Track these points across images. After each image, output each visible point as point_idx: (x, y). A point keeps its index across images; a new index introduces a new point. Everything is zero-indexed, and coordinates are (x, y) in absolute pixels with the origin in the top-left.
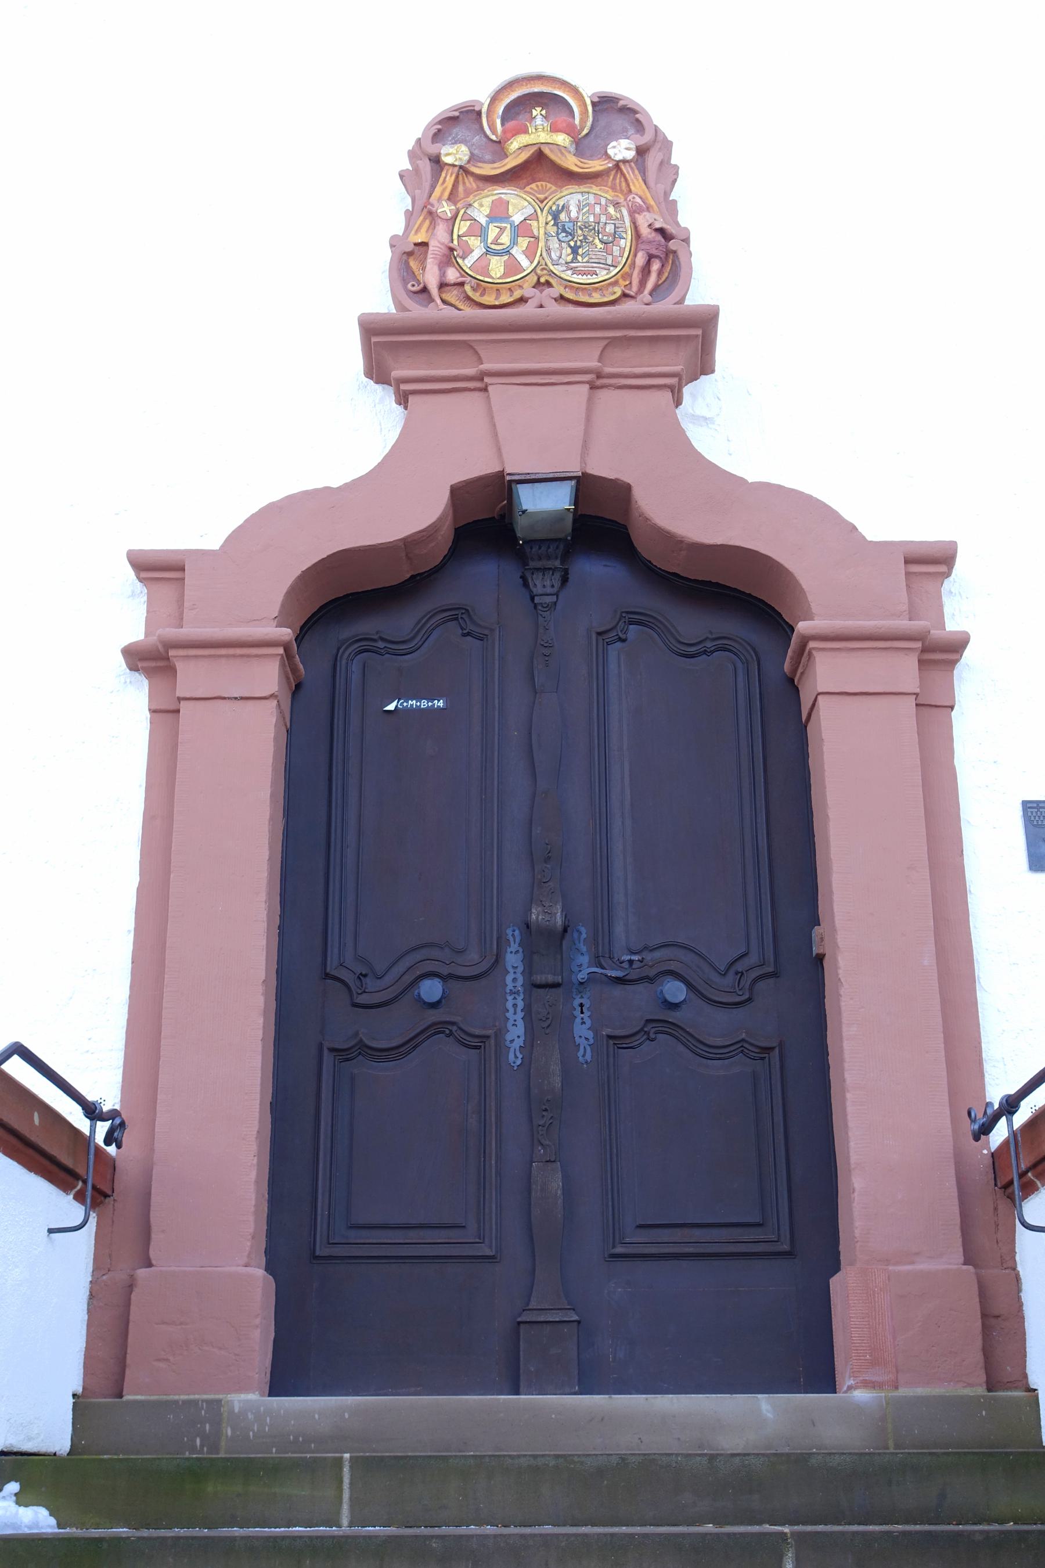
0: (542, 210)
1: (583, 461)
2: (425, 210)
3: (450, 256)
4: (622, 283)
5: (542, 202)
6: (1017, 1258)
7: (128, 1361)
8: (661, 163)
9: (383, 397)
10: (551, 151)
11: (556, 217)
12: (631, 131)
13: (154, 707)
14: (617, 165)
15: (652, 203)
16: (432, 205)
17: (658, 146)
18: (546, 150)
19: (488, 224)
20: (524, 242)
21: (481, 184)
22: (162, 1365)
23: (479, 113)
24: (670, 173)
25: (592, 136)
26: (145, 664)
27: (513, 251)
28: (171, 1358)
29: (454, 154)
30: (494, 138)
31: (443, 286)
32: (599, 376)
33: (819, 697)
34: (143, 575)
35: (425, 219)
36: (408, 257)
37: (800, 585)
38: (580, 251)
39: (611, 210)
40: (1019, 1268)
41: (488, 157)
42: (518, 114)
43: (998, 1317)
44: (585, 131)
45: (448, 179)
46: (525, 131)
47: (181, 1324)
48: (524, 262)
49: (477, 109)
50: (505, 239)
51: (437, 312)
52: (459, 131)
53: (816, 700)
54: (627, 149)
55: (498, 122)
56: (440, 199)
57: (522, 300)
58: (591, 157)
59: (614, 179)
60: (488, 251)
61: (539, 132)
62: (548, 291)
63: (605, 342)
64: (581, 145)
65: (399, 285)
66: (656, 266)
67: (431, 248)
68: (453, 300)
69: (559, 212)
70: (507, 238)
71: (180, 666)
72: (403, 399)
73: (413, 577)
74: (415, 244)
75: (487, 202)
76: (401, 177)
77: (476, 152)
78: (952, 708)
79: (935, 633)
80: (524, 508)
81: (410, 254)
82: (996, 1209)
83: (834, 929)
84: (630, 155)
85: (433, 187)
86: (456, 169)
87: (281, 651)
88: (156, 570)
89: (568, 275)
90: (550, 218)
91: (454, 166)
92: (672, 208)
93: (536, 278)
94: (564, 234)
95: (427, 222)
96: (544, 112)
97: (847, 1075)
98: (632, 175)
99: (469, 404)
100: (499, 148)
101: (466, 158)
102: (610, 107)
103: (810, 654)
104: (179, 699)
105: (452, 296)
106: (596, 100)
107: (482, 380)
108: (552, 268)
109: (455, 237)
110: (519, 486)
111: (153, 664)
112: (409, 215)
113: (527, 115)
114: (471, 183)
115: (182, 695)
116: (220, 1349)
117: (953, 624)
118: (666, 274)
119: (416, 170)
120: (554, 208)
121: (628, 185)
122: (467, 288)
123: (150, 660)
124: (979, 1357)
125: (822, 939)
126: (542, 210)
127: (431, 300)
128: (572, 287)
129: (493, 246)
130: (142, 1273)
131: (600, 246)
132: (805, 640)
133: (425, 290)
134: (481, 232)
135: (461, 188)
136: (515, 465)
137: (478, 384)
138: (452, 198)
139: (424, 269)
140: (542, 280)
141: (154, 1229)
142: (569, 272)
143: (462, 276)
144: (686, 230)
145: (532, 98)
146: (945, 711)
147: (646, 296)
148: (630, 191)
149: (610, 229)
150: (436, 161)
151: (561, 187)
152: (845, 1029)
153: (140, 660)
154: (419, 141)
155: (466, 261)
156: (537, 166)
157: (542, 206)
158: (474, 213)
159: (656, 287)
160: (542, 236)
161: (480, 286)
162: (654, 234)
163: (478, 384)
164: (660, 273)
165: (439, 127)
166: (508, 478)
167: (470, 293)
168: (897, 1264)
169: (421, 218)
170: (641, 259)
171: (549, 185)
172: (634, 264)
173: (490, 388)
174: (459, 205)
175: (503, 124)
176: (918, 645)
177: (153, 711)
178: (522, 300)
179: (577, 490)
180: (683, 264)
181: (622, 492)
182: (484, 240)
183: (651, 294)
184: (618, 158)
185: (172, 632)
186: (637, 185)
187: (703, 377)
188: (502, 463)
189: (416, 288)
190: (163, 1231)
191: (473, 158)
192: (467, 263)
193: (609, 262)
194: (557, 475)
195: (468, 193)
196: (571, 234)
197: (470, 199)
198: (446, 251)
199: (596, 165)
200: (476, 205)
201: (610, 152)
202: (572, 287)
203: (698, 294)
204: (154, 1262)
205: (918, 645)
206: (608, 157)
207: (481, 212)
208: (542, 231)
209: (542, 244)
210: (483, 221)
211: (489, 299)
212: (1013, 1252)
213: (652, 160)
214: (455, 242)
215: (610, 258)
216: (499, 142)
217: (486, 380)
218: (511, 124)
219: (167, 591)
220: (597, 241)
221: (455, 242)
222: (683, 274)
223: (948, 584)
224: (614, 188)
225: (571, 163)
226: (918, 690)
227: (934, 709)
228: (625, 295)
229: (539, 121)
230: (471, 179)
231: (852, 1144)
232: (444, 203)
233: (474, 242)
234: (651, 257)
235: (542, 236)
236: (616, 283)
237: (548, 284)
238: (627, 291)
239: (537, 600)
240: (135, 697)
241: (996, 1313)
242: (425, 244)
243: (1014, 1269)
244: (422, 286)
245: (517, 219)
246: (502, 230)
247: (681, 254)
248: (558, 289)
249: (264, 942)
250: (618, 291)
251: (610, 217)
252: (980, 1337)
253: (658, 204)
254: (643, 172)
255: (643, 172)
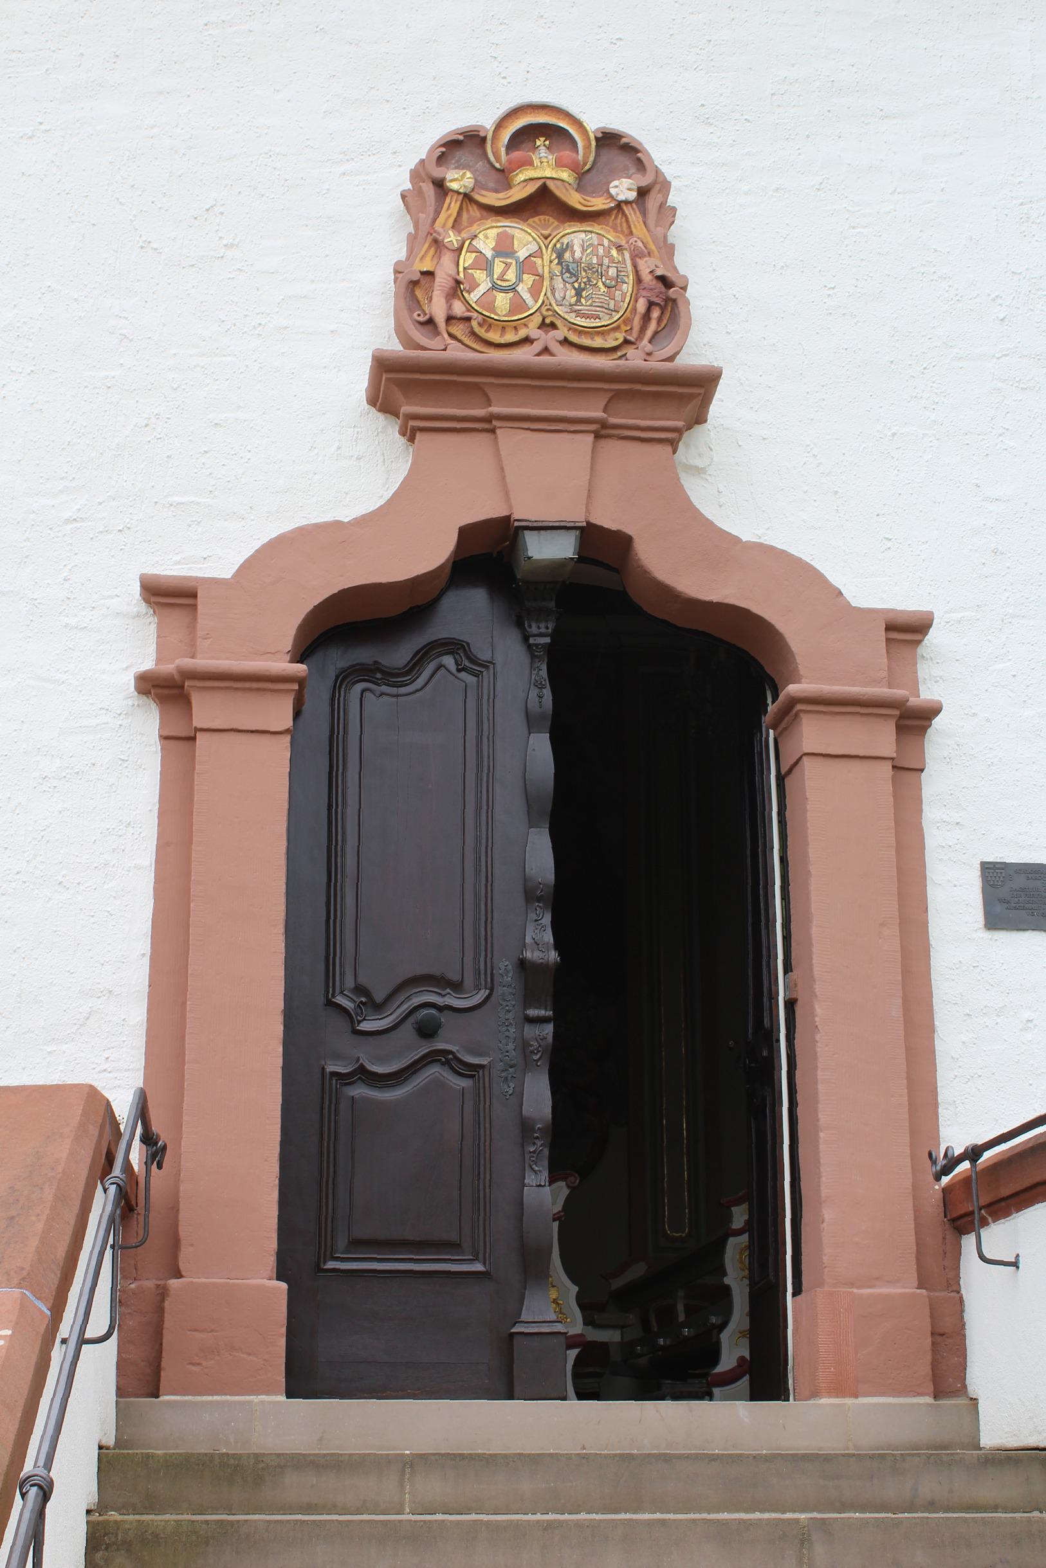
0: (547, 248)
1: (588, 511)
2: (430, 239)
3: (456, 289)
4: (624, 328)
5: (546, 238)
6: (962, 1282)
7: (163, 1364)
8: (660, 206)
9: (388, 431)
10: (557, 188)
11: (560, 256)
12: (632, 170)
13: (166, 734)
14: (619, 205)
15: (653, 247)
16: (439, 234)
17: (657, 187)
18: (551, 185)
19: (494, 258)
20: (528, 279)
21: (485, 214)
22: (194, 1368)
23: (484, 139)
24: (668, 214)
25: (594, 171)
26: (159, 691)
27: (519, 289)
28: (204, 1363)
29: (459, 179)
30: (497, 165)
31: (450, 319)
32: (604, 425)
33: (805, 758)
34: (153, 599)
35: (430, 247)
36: (413, 286)
37: (789, 647)
38: (584, 294)
39: (614, 252)
40: (963, 1292)
41: (491, 185)
42: (522, 142)
43: (942, 1335)
44: (587, 167)
45: (453, 205)
46: (530, 163)
47: (212, 1331)
48: (526, 296)
49: (482, 134)
50: (511, 275)
51: (455, 351)
52: (462, 155)
53: (801, 758)
54: (629, 189)
55: (503, 150)
56: (444, 226)
57: (527, 340)
58: (592, 194)
59: (616, 217)
60: (494, 287)
61: (543, 166)
62: (553, 333)
63: (610, 394)
64: (582, 177)
65: (405, 313)
66: (655, 314)
67: (437, 280)
68: (458, 334)
69: (565, 250)
70: (510, 271)
71: (195, 698)
72: (410, 434)
73: (411, 609)
74: (423, 273)
75: (492, 233)
76: (403, 197)
77: (479, 178)
78: (922, 770)
79: (913, 701)
80: (530, 555)
81: (415, 283)
82: (944, 1238)
83: (812, 979)
84: (632, 195)
85: (437, 213)
86: (461, 197)
87: (296, 687)
88: (169, 597)
89: (571, 317)
90: (554, 256)
91: (458, 193)
92: (669, 250)
93: (541, 319)
94: (568, 275)
95: (432, 251)
96: (547, 143)
97: (820, 1116)
98: (633, 215)
99: (475, 446)
100: (504, 177)
101: (471, 185)
102: (609, 140)
103: (797, 715)
104: (197, 730)
105: (458, 330)
106: (600, 135)
107: (490, 422)
108: (556, 308)
109: (461, 269)
110: (526, 532)
111: (166, 691)
112: (412, 240)
113: (531, 144)
114: (475, 212)
115: (199, 726)
116: (249, 1354)
117: (928, 693)
118: (665, 322)
119: (419, 193)
120: (558, 246)
121: (629, 227)
122: (474, 324)
123: (166, 690)
124: (928, 1370)
125: (796, 985)
126: (547, 248)
127: (436, 332)
128: (575, 330)
129: (499, 282)
130: (174, 1283)
131: (603, 289)
132: (793, 701)
133: (430, 322)
134: (486, 265)
135: (465, 216)
136: (523, 511)
137: (486, 426)
138: (456, 225)
139: (430, 299)
140: (548, 321)
141: (183, 1242)
142: (573, 315)
143: (468, 311)
144: (685, 278)
145: (540, 129)
146: (915, 774)
147: (645, 341)
148: (631, 233)
149: (612, 272)
150: (440, 185)
151: (563, 222)
152: (819, 1073)
153: (153, 686)
154: (422, 161)
155: (472, 295)
156: (541, 203)
157: (547, 242)
158: (479, 244)
159: (656, 333)
160: (546, 275)
161: (487, 323)
162: (654, 282)
163: (486, 426)
164: (660, 320)
165: (444, 149)
166: (516, 524)
167: (477, 329)
168: (858, 1288)
169: (427, 245)
170: (641, 306)
171: (552, 220)
172: (635, 309)
173: (498, 431)
174: (464, 235)
175: (507, 153)
176: (897, 712)
177: (165, 738)
178: (527, 340)
179: (581, 537)
180: (682, 314)
181: (622, 543)
182: (490, 274)
183: (650, 342)
184: (621, 197)
185: (187, 662)
186: (639, 229)
187: (697, 426)
188: (511, 507)
189: (421, 319)
190: (192, 1245)
191: (478, 185)
192: (473, 297)
193: (612, 306)
194: (562, 524)
195: (471, 222)
196: (575, 275)
197: (474, 229)
198: (452, 283)
199: (599, 203)
200: (481, 236)
201: (613, 191)
202: (575, 330)
203: (697, 350)
204: (183, 1273)
205: (897, 712)
206: (611, 197)
207: (486, 244)
208: (546, 269)
209: (546, 283)
210: (489, 254)
211: (494, 336)
212: (957, 1277)
213: (652, 203)
214: (462, 275)
215: (612, 304)
216: (502, 171)
217: (495, 423)
218: (516, 155)
219: (177, 618)
220: (600, 284)
221: (462, 275)
222: (682, 322)
223: (922, 650)
224: (615, 230)
225: (574, 199)
226: (894, 755)
227: (907, 770)
228: (626, 342)
229: (543, 152)
230: (475, 207)
231: (823, 1179)
232: (451, 233)
233: (480, 275)
234: (651, 304)
235: (546, 275)
236: (617, 328)
237: (553, 326)
238: (629, 338)
239: (531, 641)
240: (148, 722)
241: (942, 1332)
242: (429, 274)
243: (959, 1292)
244: (427, 317)
245: (522, 254)
246: (508, 265)
247: (680, 303)
248: (562, 332)
249: (283, 973)
250: (620, 336)
251: (612, 260)
252: (930, 1353)
253: (659, 248)
254: (644, 213)
255: (644, 213)
